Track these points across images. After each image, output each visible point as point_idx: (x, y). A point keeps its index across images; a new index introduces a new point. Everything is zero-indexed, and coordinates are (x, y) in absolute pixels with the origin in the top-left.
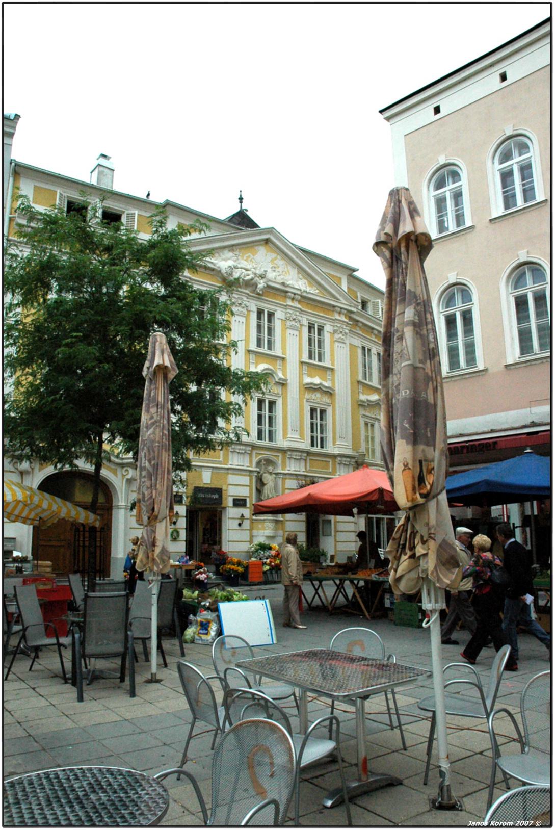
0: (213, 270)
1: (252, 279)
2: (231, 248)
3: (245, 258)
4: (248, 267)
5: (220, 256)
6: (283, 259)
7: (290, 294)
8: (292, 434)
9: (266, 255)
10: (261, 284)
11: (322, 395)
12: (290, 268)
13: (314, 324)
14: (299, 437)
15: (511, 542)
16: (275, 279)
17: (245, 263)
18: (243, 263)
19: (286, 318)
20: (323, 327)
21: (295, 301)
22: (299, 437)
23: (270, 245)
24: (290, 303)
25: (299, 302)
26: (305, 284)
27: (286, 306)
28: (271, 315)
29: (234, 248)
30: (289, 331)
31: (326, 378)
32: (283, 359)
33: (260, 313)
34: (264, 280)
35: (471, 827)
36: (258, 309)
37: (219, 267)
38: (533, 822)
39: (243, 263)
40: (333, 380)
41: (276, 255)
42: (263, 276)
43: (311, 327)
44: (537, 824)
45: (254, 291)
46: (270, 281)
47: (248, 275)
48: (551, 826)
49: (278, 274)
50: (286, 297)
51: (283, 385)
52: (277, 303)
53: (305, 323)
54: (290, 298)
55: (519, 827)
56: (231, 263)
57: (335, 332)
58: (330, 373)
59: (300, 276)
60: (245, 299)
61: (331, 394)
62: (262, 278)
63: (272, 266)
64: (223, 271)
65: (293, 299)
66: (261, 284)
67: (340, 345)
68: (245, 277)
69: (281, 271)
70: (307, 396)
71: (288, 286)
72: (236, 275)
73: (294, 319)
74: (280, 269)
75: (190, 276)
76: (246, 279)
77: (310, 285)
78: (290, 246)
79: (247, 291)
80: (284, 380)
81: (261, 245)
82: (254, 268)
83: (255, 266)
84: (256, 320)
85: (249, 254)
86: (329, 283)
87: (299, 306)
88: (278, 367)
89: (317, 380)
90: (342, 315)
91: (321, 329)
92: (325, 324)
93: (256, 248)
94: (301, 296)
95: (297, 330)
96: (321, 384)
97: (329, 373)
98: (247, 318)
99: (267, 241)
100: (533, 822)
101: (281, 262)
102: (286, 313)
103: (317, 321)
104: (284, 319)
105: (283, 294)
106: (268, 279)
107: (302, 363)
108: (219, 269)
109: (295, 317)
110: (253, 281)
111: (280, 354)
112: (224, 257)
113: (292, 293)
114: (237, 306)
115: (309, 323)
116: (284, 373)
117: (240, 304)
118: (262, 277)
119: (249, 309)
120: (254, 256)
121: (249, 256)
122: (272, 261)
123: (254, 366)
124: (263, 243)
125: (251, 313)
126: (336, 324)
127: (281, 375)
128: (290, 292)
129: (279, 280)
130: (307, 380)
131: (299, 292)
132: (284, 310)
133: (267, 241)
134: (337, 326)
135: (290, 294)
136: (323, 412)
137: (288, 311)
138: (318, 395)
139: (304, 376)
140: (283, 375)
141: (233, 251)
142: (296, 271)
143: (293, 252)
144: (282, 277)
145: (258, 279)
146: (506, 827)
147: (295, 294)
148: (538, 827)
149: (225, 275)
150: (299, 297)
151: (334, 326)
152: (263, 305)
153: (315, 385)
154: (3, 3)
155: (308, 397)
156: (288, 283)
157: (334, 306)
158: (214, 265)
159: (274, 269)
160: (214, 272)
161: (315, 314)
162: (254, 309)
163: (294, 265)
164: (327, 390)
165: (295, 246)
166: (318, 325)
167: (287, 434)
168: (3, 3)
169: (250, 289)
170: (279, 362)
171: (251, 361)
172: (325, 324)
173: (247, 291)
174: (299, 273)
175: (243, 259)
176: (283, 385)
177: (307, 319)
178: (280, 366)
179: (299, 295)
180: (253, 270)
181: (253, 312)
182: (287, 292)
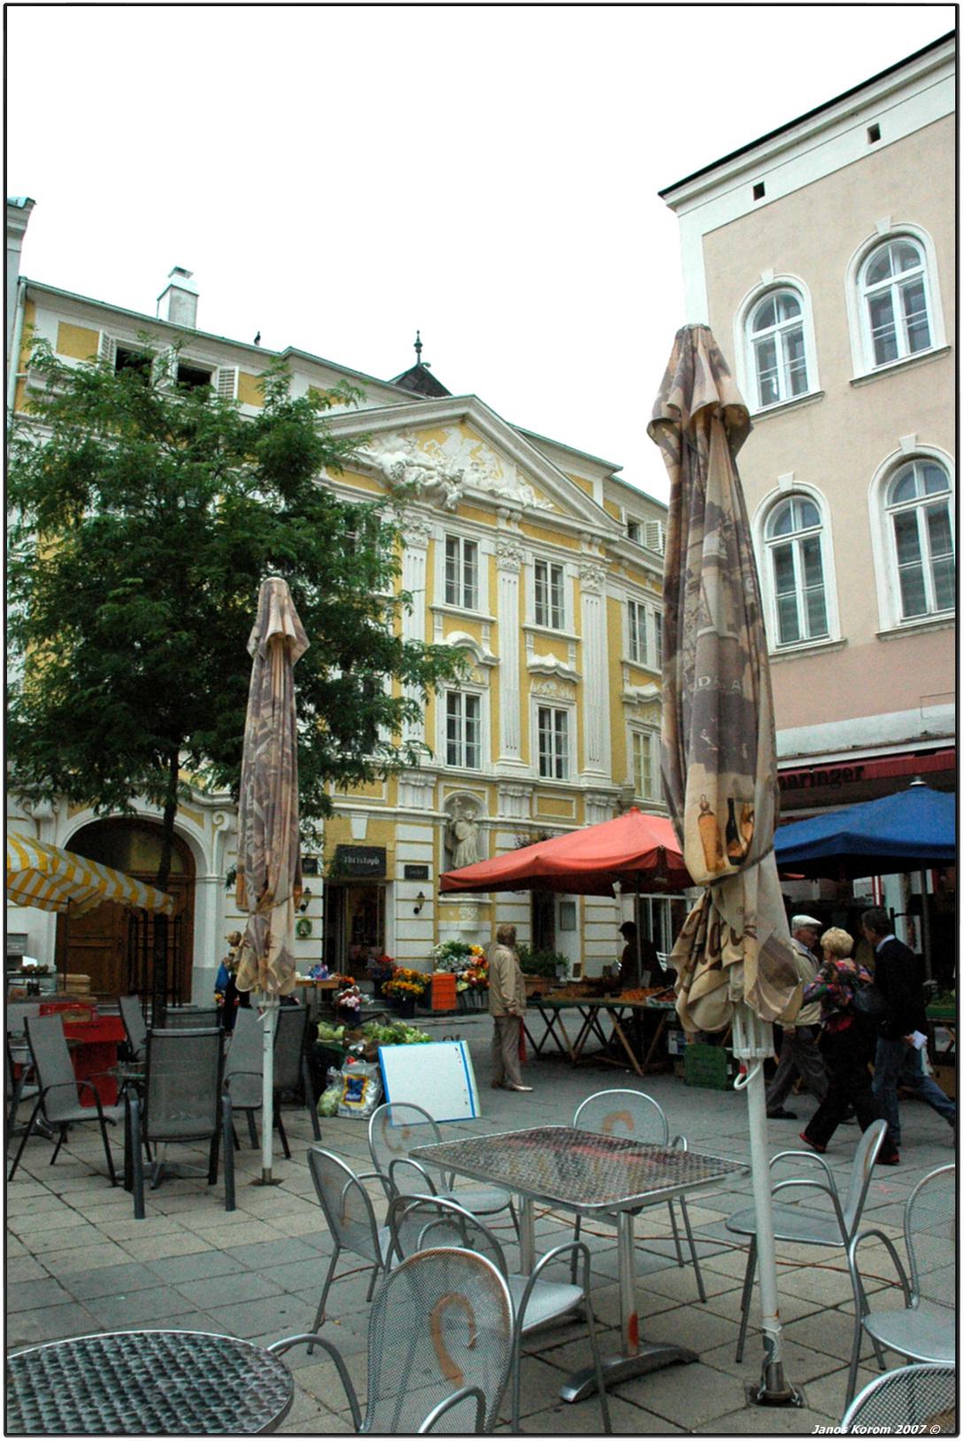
0: (370, 468)
1: (438, 485)
2: (402, 430)
3: (425, 448)
4: (431, 464)
5: (381, 444)
6: (491, 449)
7: (503, 510)
8: (507, 754)
9: (462, 443)
10: (454, 493)
11: (559, 685)
12: (503, 465)
13: (545, 563)
15: (888, 942)
16: (478, 484)
17: (426, 456)
18: (423, 457)
19: (497, 553)
20: (561, 568)
21: (512, 523)
23: (469, 425)
24: (503, 525)
25: (520, 524)
26: (530, 492)
28: (470, 547)
29: (407, 430)
30: (502, 575)
31: (567, 656)
33: (451, 543)
34: (459, 486)
35: (817, 1435)
36: (447, 536)
37: (380, 464)
38: (925, 1426)
39: (423, 457)
40: (578, 660)
41: (479, 443)
42: (456, 479)
43: (540, 568)
44: (932, 1431)
45: (441, 505)
46: (469, 487)
47: (431, 478)
48: (956, 1433)
49: (483, 475)
50: (496, 515)
51: (491, 668)
52: (482, 527)
53: (531, 560)
54: (503, 517)
55: (902, 1435)
56: (401, 456)
57: (582, 576)
59: (522, 479)
60: (425, 518)
61: (575, 684)
62: (455, 482)
63: (472, 461)
64: (388, 471)
65: (509, 519)
66: (454, 493)
67: (591, 598)
68: (425, 481)
69: (488, 471)
70: (534, 687)
71: (500, 497)
72: (410, 478)
73: (511, 554)
74: (487, 468)
75: (330, 479)
76: (427, 484)
77: (539, 494)
78: (504, 428)
79: (429, 506)
80: (493, 660)
81: (453, 425)
82: (441, 466)
83: (443, 462)
85: (433, 441)
86: (571, 491)
87: (520, 532)
88: (483, 637)
89: (550, 661)
91: (557, 572)
92: (565, 563)
93: (445, 430)
94: (523, 514)
95: (516, 573)
96: (557, 667)
97: (571, 647)
98: (430, 552)
99: (464, 419)
100: (925, 1426)
101: (487, 455)
102: (497, 544)
103: (551, 558)
104: (493, 553)
105: (492, 511)
106: (465, 484)
107: (525, 630)
108: (380, 467)
109: (512, 550)
110: (440, 488)
111: (486, 615)
112: (388, 446)
113: (507, 508)
114: (411, 531)
115: (536, 561)
116: (494, 648)
117: (417, 528)
118: (455, 480)
119: (433, 537)
120: (441, 444)
121: (433, 445)
122: (473, 453)
123: (441, 635)
124: (457, 421)
125: (436, 543)
126: (583, 563)
127: (487, 651)
128: (504, 507)
129: (485, 486)
130: (534, 660)
131: (519, 508)
132: (493, 539)
133: (464, 419)
134: (585, 566)
136: (561, 715)
137: (501, 539)
138: (553, 686)
139: (528, 652)
140: (492, 650)
141: (404, 435)
142: (514, 470)
143: (510, 437)
144: (490, 480)
145: (447, 484)
146: (879, 1435)
147: (512, 510)
148: (934, 1435)
149: (391, 477)
150: (520, 516)
151: (579, 566)
152: (456, 530)
154: (6, 6)
155: (535, 690)
156: (500, 491)
157: (580, 532)
158: (372, 460)
159: (476, 467)
160: (372, 472)
161: (548, 546)
162: (442, 536)
163: (511, 461)
164: (568, 677)
165: (512, 426)
166: (552, 565)
167: (499, 754)
168: (6, 6)
169: (435, 501)
170: (484, 629)
171: (436, 627)
172: (565, 563)
173: (429, 506)
174: (519, 474)
175: (422, 449)
176: (491, 668)
177: (534, 554)
178: (486, 635)
179: (519, 512)
180: (439, 468)
181: (440, 541)
182: (498, 507)
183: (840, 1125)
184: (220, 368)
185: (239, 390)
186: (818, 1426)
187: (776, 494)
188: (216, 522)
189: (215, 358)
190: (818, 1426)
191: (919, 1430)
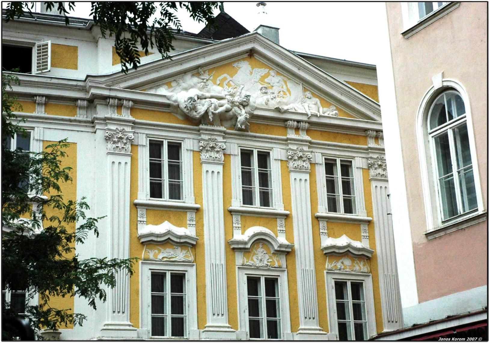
0: (168, 106)
1: (227, 111)
2: (196, 71)
3: (218, 82)
4: (222, 95)
5: (178, 84)
6: (278, 73)
7: (290, 123)
8: (306, 324)
9: (251, 73)
10: (243, 115)
11: (353, 261)
12: (290, 85)
13: (336, 160)
14: (228, 325)
16: (267, 104)
17: (219, 88)
18: (216, 90)
19: (288, 158)
20: (351, 162)
21: (300, 132)
22: (228, 325)
23: (256, 56)
24: (292, 135)
25: (308, 131)
26: (316, 104)
27: (367, 149)
28: (264, 158)
29: (200, 70)
30: (293, 176)
31: (360, 236)
32: (369, 223)
33: (246, 156)
34: (248, 109)
35: (440, 341)
36: (241, 150)
37: (176, 101)
39: (216, 90)
40: (371, 238)
41: (267, 70)
42: (244, 103)
43: (330, 167)
45: (234, 127)
46: (256, 108)
47: (222, 106)
49: (272, 96)
50: (286, 127)
51: (288, 253)
52: (272, 139)
53: (321, 160)
54: (291, 128)
56: (194, 93)
57: (370, 166)
58: (194, 215)
59: (308, 94)
60: (220, 139)
61: (369, 259)
62: (244, 107)
63: (261, 86)
64: (182, 106)
65: (297, 129)
66: (243, 115)
67: (379, 184)
68: (216, 109)
69: (276, 92)
70: (328, 265)
71: (286, 112)
72: (201, 109)
73: (300, 158)
74: (276, 90)
75: (134, 119)
76: (217, 112)
77: (324, 103)
78: (287, 55)
79: (223, 129)
80: (287, 247)
81: (243, 59)
82: (231, 95)
83: (232, 91)
84: (325, 175)
85: (225, 75)
86: (354, 98)
87: (305, 137)
88: (279, 228)
89: (343, 241)
90: (289, 131)
91: (346, 168)
92: (353, 157)
93: (235, 65)
94: (309, 123)
95: (306, 173)
96: (349, 246)
97: (363, 227)
98: (226, 166)
99: (251, 53)
101: (275, 79)
102: (287, 150)
103: (339, 155)
104: (284, 159)
105: (281, 124)
106: (252, 106)
107: (317, 219)
108: (176, 104)
109: (300, 154)
110: (231, 113)
111: (282, 211)
112: (184, 85)
113: (294, 120)
114: (207, 151)
115: (325, 159)
116: (289, 237)
117: (213, 148)
118: (244, 104)
119: (228, 153)
120: (232, 76)
121: (225, 79)
122: (262, 79)
123: (240, 231)
124: (246, 55)
125: (140, 149)
126: (371, 155)
127: (282, 239)
128: (291, 120)
129: (273, 104)
130: (327, 242)
131: (305, 118)
132: (284, 147)
133: (251, 53)
134: (371, 158)
135: (370, 132)
136: (357, 288)
137: (291, 146)
138: (347, 262)
139: (322, 237)
140: (287, 239)
141: (198, 74)
142: (300, 88)
143: (292, 61)
144: (278, 100)
145: (236, 108)
147: (298, 121)
148: (480, 341)
149: (185, 110)
150: (307, 125)
151: (367, 158)
152: (248, 144)
153: (158, 236)
154: (2, 2)
155: (330, 267)
156: (285, 108)
157: (366, 130)
158: (168, 99)
159: (265, 91)
160: (170, 108)
161: (335, 146)
162: (237, 151)
163: (297, 80)
164: (360, 253)
165: (293, 53)
166: (341, 161)
167: (298, 325)
169: (229, 124)
170: (280, 223)
171: (234, 225)
172: (353, 157)
173: (223, 129)
174: (305, 90)
175: (215, 83)
176: (288, 253)
177: (323, 154)
178: (281, 226)
179: (306, 122)
180: (228, 97)
181: (144, 146)
182: (286, 120)
183: (166, 222)
184: (38, 43)
185: (52, 58)
186: (440, 338)
187: (432, 92)
188: (162, 42)
189: (31, 36)
190: (440, 338)
191: (475, 339)
